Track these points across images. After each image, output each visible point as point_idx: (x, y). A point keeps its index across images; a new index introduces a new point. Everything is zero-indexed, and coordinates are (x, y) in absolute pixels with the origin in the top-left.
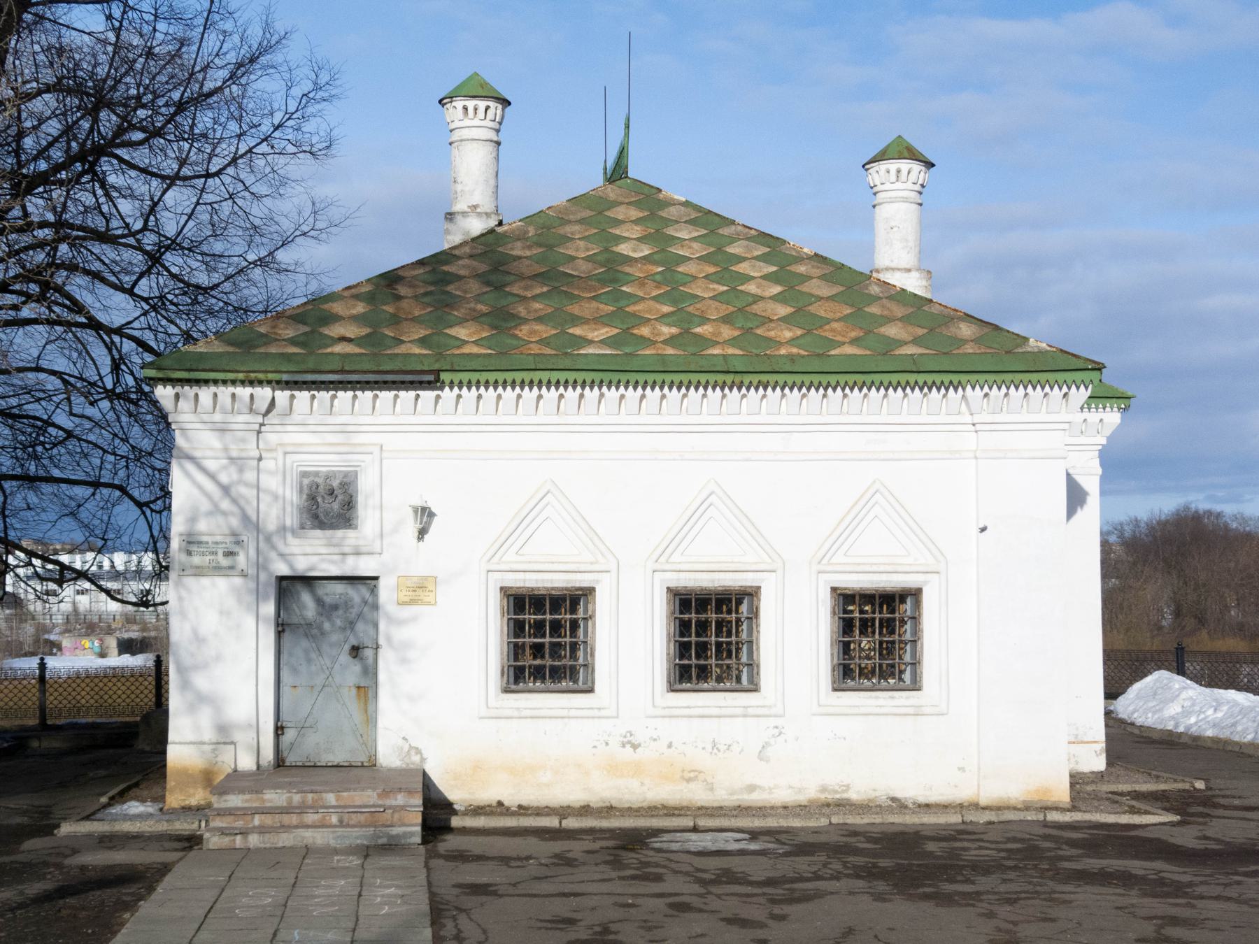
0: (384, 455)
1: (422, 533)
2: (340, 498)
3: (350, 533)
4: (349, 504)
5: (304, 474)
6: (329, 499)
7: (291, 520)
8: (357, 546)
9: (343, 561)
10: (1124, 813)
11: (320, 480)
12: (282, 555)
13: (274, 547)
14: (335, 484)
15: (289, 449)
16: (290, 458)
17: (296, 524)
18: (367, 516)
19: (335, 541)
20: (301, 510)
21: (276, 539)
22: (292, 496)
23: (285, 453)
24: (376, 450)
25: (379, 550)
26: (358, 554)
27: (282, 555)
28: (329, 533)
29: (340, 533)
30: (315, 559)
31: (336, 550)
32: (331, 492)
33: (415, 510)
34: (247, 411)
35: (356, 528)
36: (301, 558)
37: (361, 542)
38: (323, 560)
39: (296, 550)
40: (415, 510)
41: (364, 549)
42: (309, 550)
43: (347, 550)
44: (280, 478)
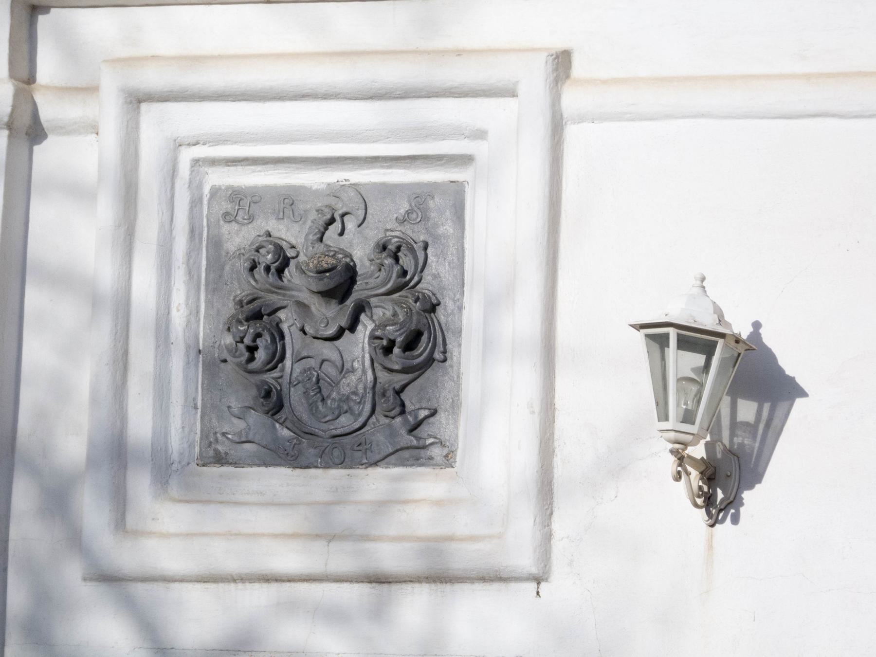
0: (572, 99)
1: (722, 481)
2: (383, 310)
3: (424, 484)
4: (419, 345)
5: (241, 204)
6: (330, 315)
7: (162, 407)
8: (434, 545)
9: (378, 613)
10: (201, 449)
11: (293, 234)
12: (108, 578)
13: (76, 540)
14: (359, 248)
15: (152, 78)
16: (157, 125)
17: (181, 432)
18: (490, 390)
19: (346, 516)
20: (211, 364)
21: (92, 511)
22: (175, 305)
23: (137, 100)
24: (533, 78)
25: (524, 560)
26: (440, 577)
27: (108, 578)
28: (321, 481)
29: (374, 482)
30: (256, 597)
31: (341, 559)
32: (340, 283)
33: (656, 335)
34: (680, 376)
35: (448, 460)
36: (196, 597)
37: (462, 523)
38: (291, 607)
39: (166, 557)
40: (656, 335)
41: (464, 557)
42: (226, 557)
43: (389, 557)
44: (106, 210)
